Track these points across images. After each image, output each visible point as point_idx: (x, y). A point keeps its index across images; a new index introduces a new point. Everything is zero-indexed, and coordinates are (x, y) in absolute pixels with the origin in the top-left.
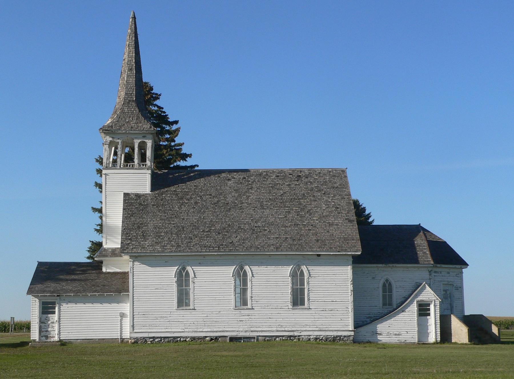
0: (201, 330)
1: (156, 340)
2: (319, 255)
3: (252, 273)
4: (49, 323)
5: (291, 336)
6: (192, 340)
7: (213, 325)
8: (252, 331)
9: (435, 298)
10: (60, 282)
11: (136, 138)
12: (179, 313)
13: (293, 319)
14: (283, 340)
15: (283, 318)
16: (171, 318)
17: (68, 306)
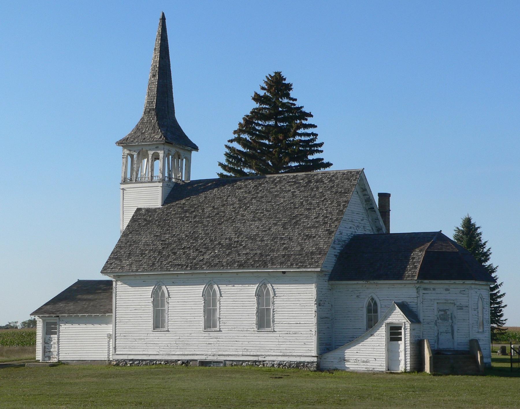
0: (174, 353)
1: (136, 363)
2: (284, 273)
3: (220, 292)
4: (52, 343)
5: (255, 362)
7: (185, 347)
9: (405, 321)
11: (150, 150)
13: (259, 343)
15: (248, 342)
16: (148, 340)
17: (65, 326)
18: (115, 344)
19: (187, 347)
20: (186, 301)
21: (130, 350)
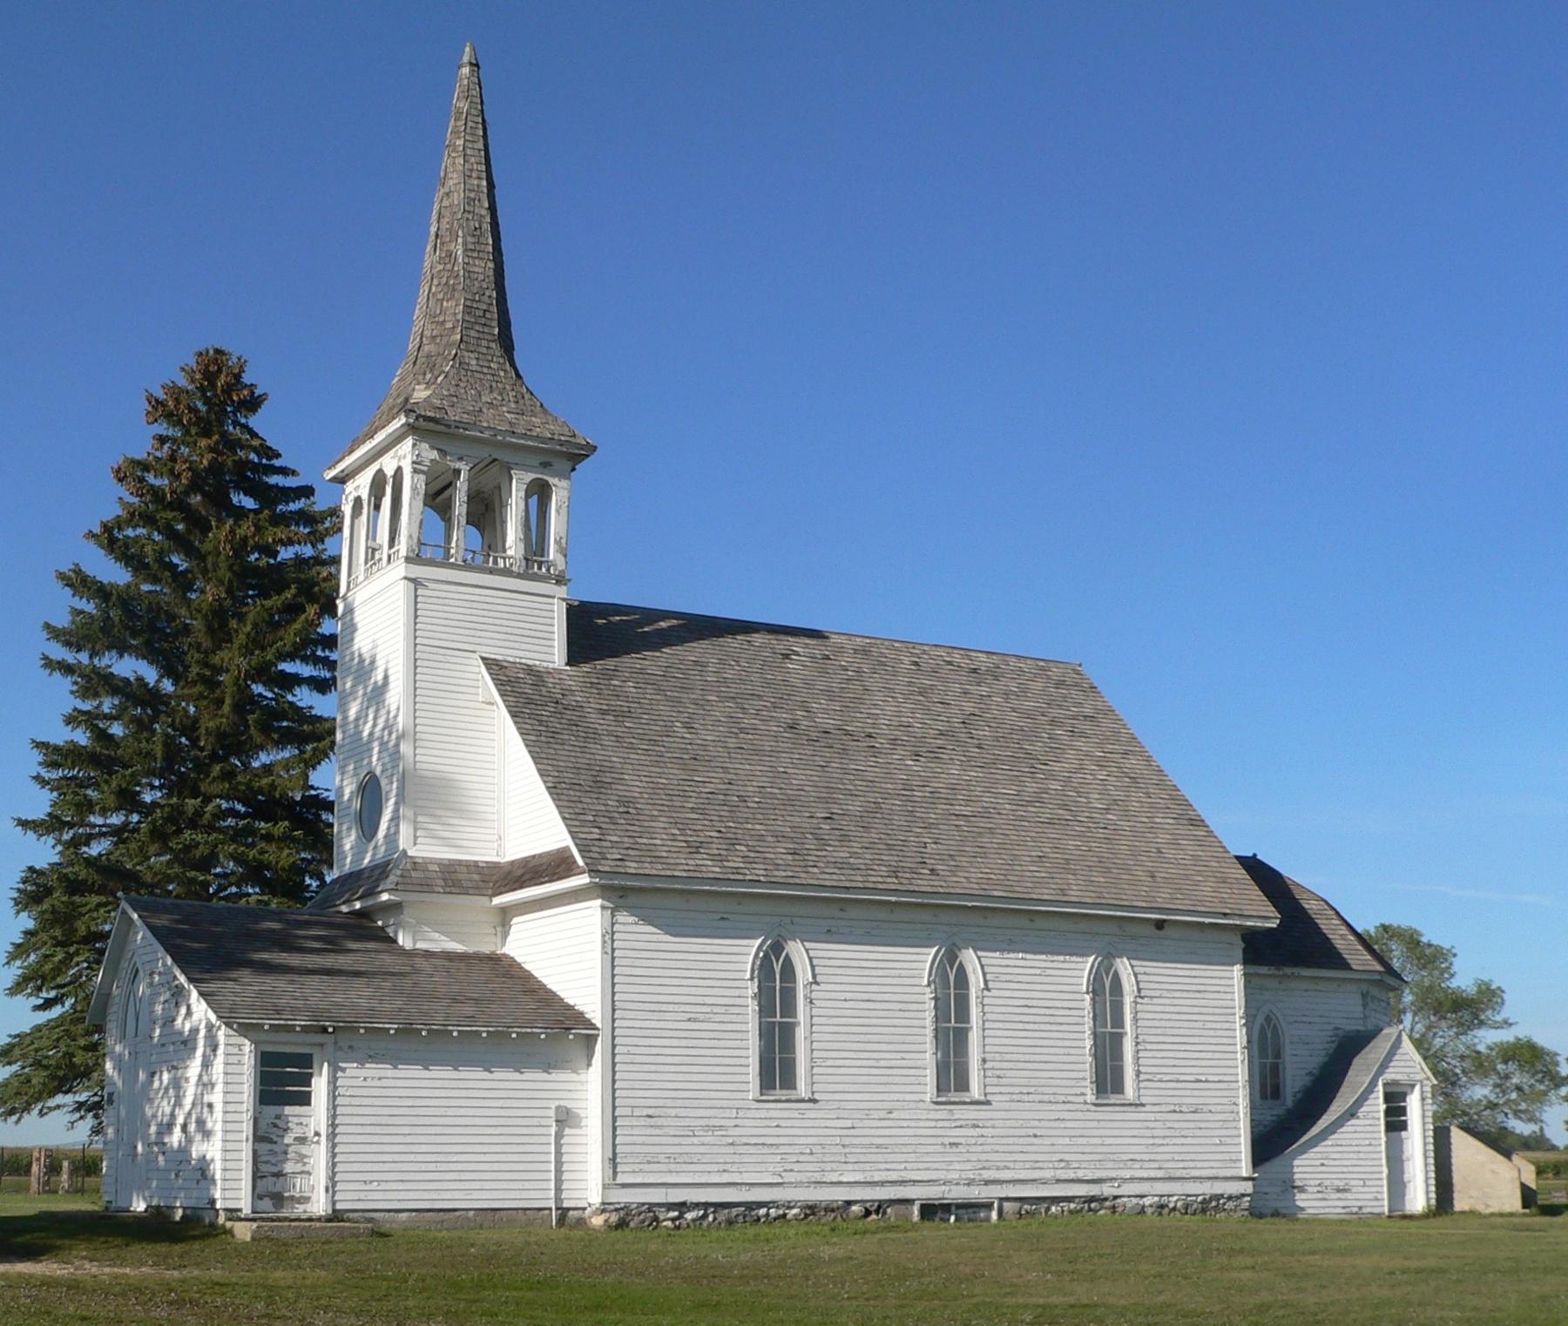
0: (834, 1177)
1: (689, 1216)
4: (286, 1141)
5: (1092, 1199)
6: (806, 1216)
8: (987, 1182)
10: (234, 975)
11: (526, 468)
12: (763, 1114)
13: (1098, 1141)
14: (1071, 1212)
16: (737, 1131)
17: (363, 1073)
18: (614, 1146)
19: (880, 1158)
20: (873, 997)
21: (673, 1167)
